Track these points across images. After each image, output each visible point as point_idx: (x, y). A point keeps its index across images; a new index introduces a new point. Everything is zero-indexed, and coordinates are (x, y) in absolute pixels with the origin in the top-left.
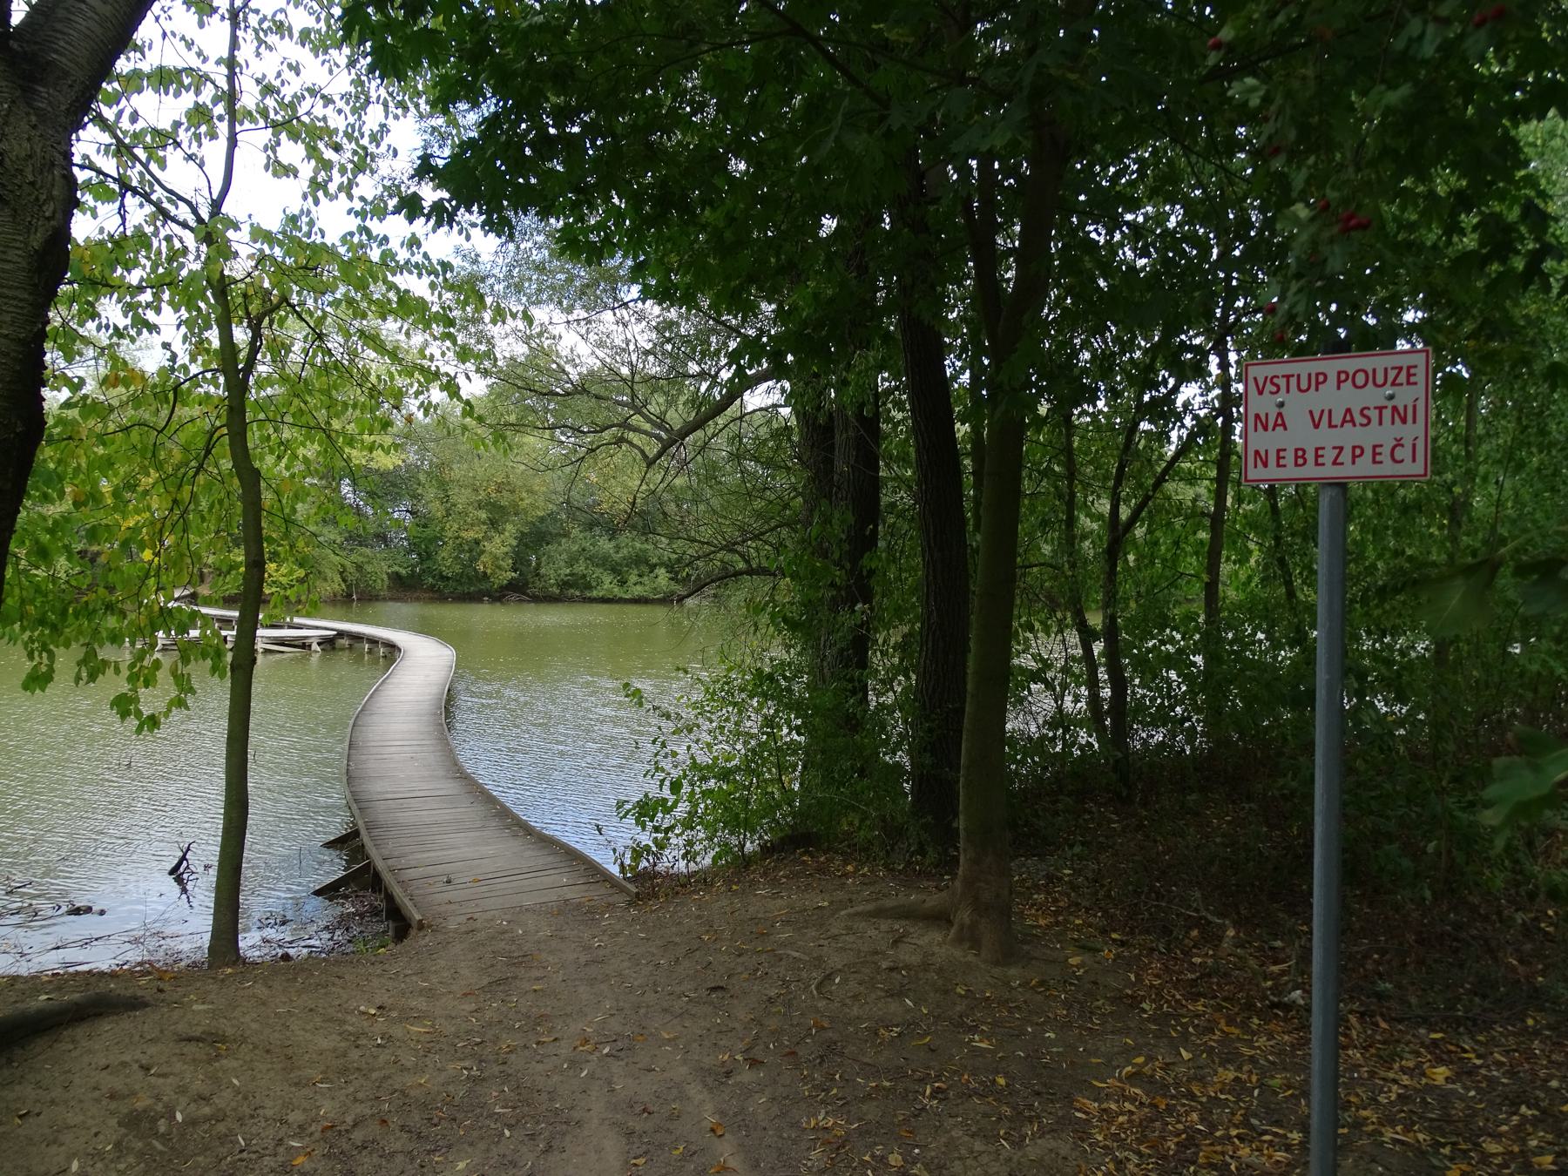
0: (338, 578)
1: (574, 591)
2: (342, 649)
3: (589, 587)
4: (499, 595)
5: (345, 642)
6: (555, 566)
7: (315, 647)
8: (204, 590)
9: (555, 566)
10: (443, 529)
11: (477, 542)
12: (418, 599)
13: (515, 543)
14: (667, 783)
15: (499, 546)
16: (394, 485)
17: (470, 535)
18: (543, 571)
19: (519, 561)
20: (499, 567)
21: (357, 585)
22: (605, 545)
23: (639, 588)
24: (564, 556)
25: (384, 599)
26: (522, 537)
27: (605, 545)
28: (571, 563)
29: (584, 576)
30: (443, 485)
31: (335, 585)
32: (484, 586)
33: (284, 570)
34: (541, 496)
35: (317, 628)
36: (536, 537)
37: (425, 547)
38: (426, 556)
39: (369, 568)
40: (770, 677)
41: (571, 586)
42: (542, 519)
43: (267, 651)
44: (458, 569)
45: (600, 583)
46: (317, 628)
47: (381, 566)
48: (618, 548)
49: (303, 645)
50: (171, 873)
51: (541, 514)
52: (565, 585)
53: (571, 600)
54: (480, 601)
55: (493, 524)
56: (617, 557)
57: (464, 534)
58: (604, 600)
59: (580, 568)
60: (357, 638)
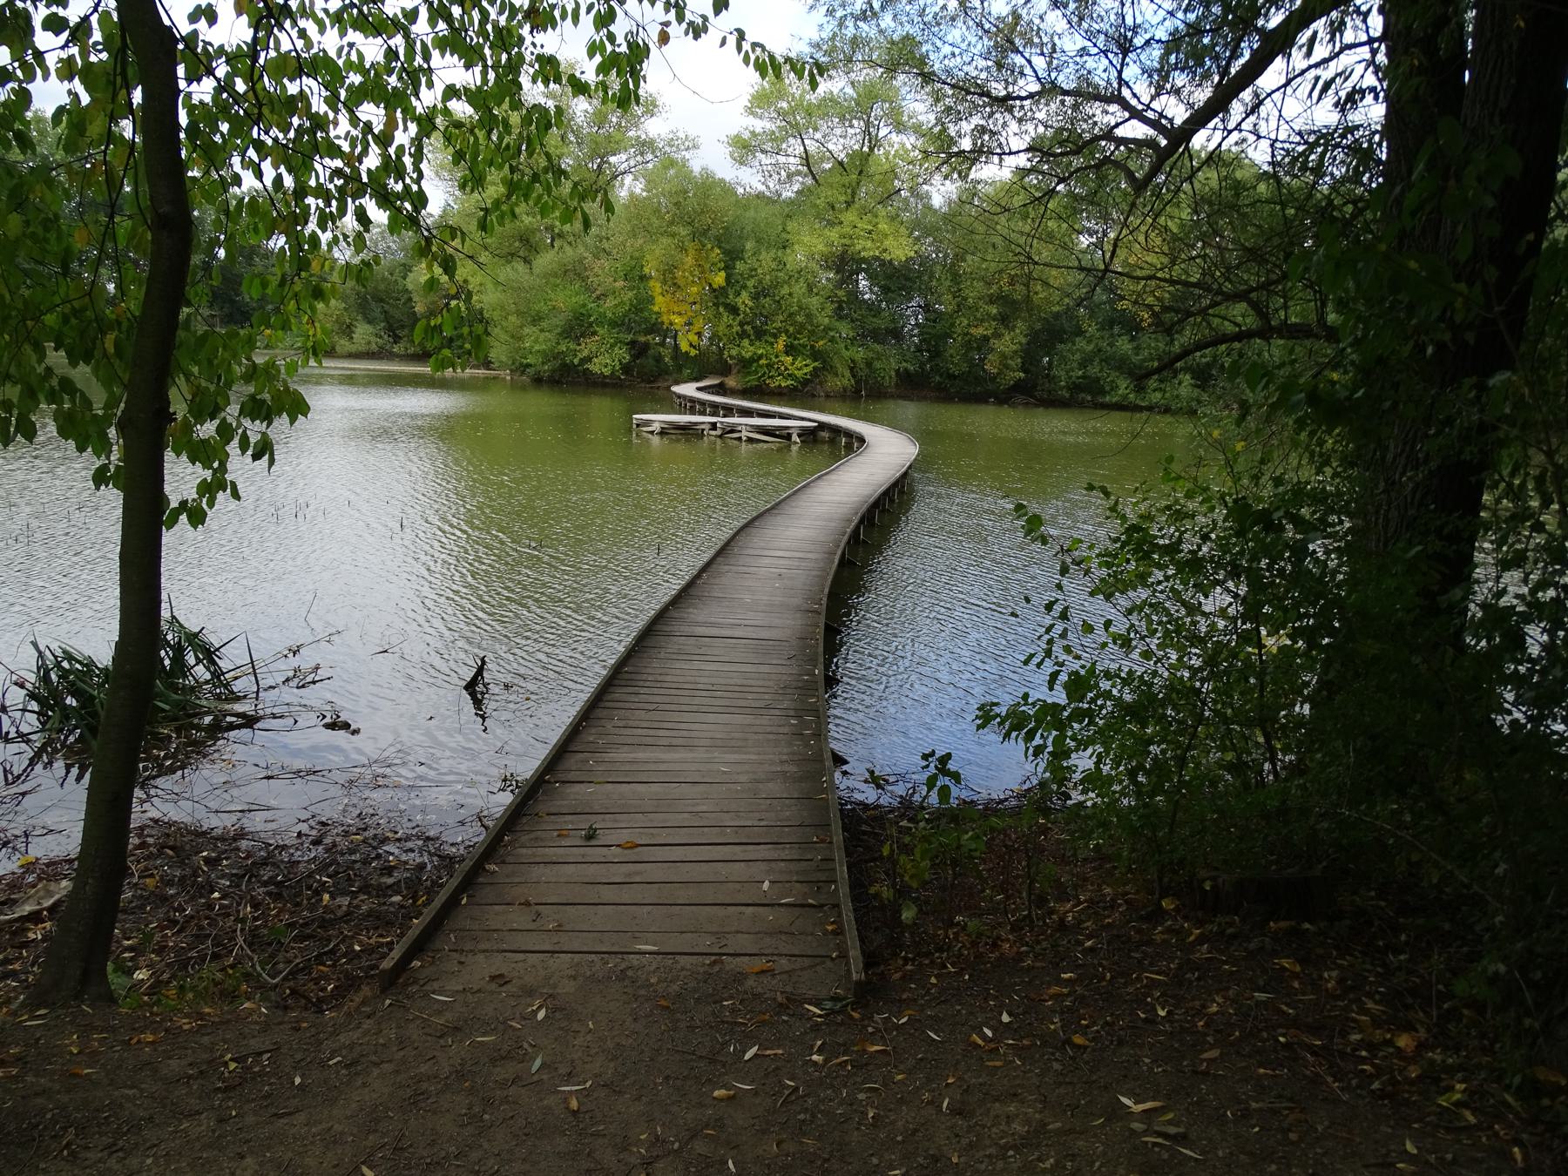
0: (848, 374)
1: (1084, 396)
2: (823, 442)
3: (1103, 393)
4: (1005, 397)
5: (825, 435)
6: (1065, 368)
7: (795, 438)
8: (731, 382)
9: (1065, 368)
10: (953, 325)
11: (986, 339)
12: (924, 398)
13: (1024, 341)
14: (1063, 677)
15: (1009, 343)
16: (908, 279)
17: (979, 331)
18: (1055, 372)
19: (1029, 357)
20: (1007, 367)
21: (866, 382)
22: (1124, 345)
23: (1158, 395)
24: (1077, 356)
25: (892, 396)
26: (1034, 336)
27: (1124, 345)
28: (1083, 364)
29: (1098, 379)
30: (956, 278)
31: (843, 380)
32: (991, 387)
33: (798, 364)
34: (1057, 287)
35: (803, 419)
36: (1052, 334)
37: (934, 340)
38: (936, 354)
39: (877, 365)
40: (1265, 519)
41: (1082, 391)
42: (1057, 316)
43: (750, 440)
44: (965, 367)
45: (1115, 388)
46: (803, 419)
47: (891, 363)
48: (1137, 349)
49: (783, 435)
50: (466, 688)
51: (1056, 309)
52: (1075, 388)
53: (1081, 405)
54: (986, 402)
55: (1004, 320)
56: (1136, 359)
57: (973, 331)
58: (1119, 407)
59: (1094, 370)
60: (836, 431)
